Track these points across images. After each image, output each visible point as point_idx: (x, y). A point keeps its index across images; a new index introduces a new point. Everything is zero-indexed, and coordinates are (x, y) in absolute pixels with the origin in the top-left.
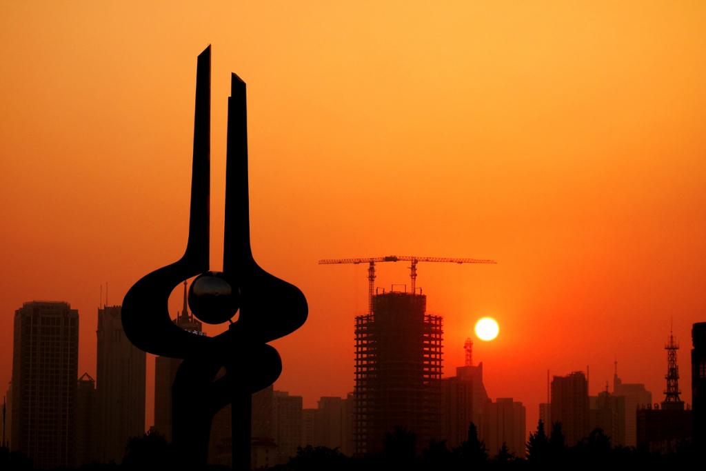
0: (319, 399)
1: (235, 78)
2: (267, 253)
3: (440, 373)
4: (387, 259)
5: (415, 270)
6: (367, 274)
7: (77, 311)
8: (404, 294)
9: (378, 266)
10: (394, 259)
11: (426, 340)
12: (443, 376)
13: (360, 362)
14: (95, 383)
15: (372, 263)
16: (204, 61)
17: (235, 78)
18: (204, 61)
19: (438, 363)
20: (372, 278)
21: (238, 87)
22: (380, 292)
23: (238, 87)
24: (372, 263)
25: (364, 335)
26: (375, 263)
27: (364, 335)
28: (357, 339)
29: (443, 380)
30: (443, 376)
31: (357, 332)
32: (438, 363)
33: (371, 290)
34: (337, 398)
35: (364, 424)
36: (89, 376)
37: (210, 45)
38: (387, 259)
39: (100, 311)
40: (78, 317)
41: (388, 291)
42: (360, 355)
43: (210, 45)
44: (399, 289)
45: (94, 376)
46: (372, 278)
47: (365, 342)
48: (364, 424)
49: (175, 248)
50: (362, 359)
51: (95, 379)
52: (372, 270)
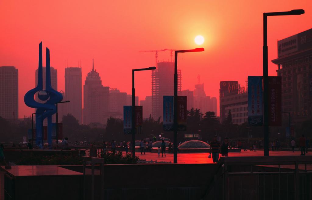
3: (181, 89)
5: (172, 54)
7: (56, 70)
8: (168, 62)
9: (158, 53)
10: (165, 50)
11: (189, 133)
12: (182, 90)
13: (153, 79)
14: (65, 94)
15: (157, 52)
16: (41, 45)
18: (41, 45)
19: (180, 81)
20: (157, 57)
21: (48, 51)
22: (160, 62)
23: (48, 51)
24: (157, 52)
25: (155, 76)
26: (158, 52)
27: (155, 76)
28: (152, 78)
30: (182, 90)
31: (152, 75)
32: (180, 88)
33: (156, 61)
35: (155, 93)
36: (62, 91)
39: (65, 69)
40: (57, 72)
41: (162, 61)
42: (153, 83)
44: (166, 61)
45: (64, 91)
46: (157, 57)
47: (155, 79)
48: (155, 99)
50: (154, 82)
51: (65, 92)
52: (156, 54)
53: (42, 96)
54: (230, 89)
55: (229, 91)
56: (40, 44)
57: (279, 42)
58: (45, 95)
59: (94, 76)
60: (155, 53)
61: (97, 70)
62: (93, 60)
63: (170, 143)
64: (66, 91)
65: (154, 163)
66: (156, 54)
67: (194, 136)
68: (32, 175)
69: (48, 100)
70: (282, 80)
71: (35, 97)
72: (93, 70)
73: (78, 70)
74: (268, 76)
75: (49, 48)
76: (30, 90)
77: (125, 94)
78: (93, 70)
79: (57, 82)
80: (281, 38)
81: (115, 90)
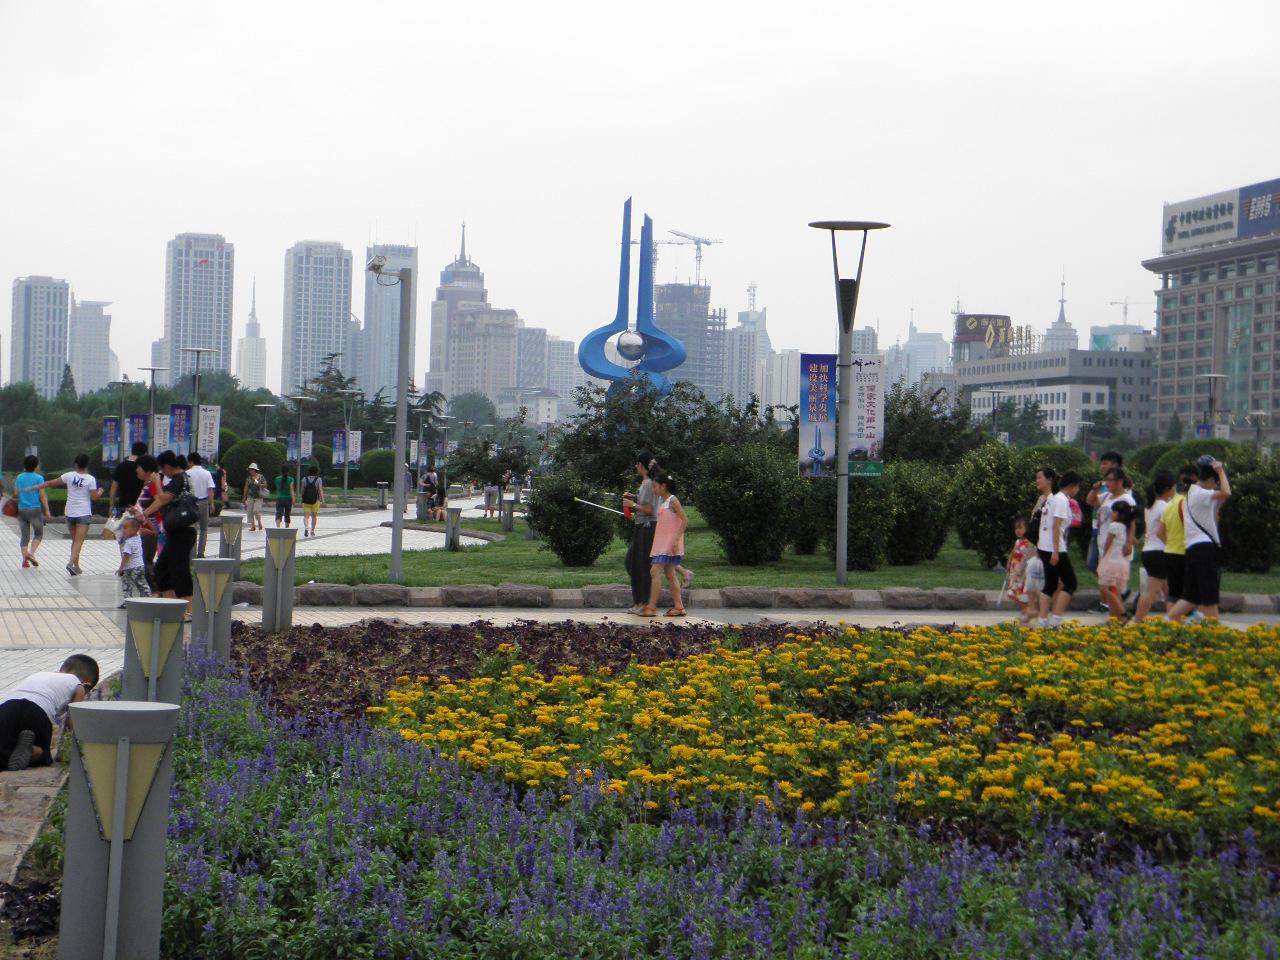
16: (628, 205)
18: (628, 205)
21: (648, 222)
23: (648, 222)
39: (369, 250)
52: (1126, 308)
53: (628, 347)
54: (992, 339)
55: (989, 345)
57: (1167, 208)
58: (638, 346)
59: (462, 277)
61: (475, 257)
62: (1062, 301)
66: (1126, 308)
68: (1121, 323)
70: (815, 773)
71: (612, 355)
72: (463, 255)
75: (651, 216)
77: (937, 337)
78: (463, 255)
79: (231, 314)
80: (1174, 200)
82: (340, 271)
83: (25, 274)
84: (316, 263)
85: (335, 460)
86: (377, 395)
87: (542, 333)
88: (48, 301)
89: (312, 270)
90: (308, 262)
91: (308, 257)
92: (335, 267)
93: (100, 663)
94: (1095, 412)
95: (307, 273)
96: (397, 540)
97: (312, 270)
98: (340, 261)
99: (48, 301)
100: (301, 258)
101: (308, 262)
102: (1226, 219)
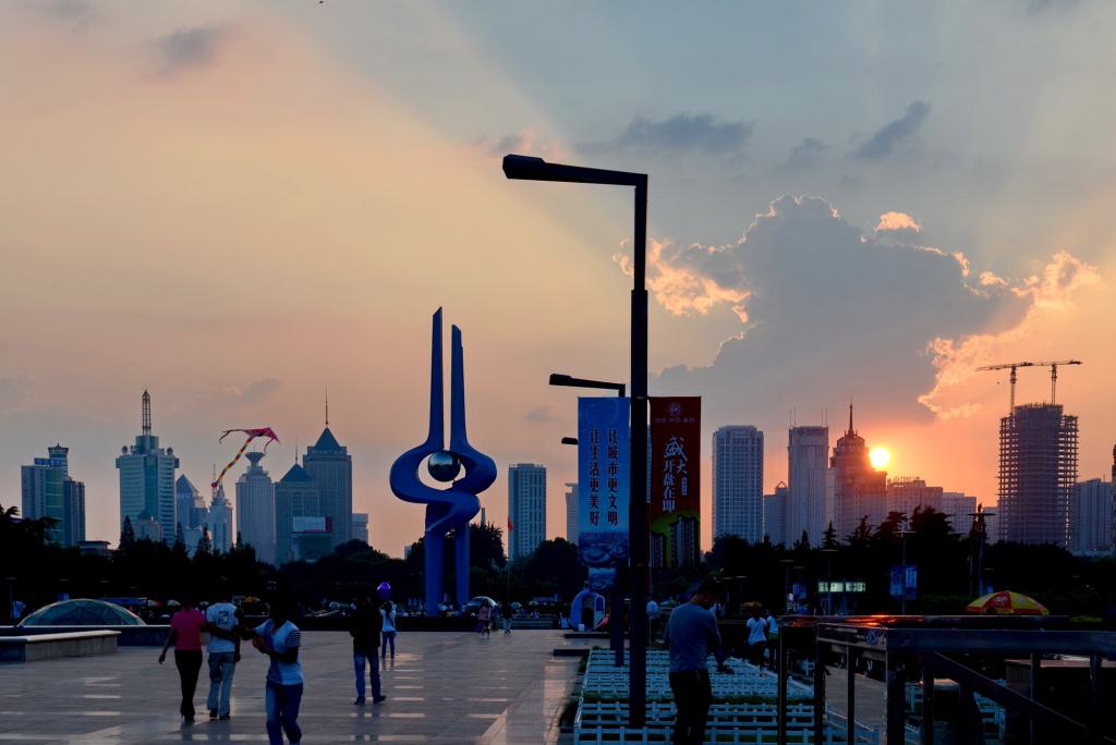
0: (495, 527)
1: (454, 327)
2: (476, 440)
4: (1025, 365)
6: (1009, 377)
11: (830, 580)
15: (1054, 366)
16: (437, 318)
17: (454, 327)
18: (437, 318)
21: (456, 333)
23: (456, 333)
29: (1079, 484)
30: (1079, 480)
31: (1001, 432)
34: (1092, 481)
37: (441, 308)
38: (1025, 365)
43: (441, 308)
49: (421, 436)
50: (1006, 455)
52: (1013, 373)
56: (434, 316)
60: (1010, 370)
63: (457, 607)
64: (790, 484)
65: (840, 645)
67: (845, 586)
69: (456, 479)
72: (851, 430)
73: (821, 432)
74: (634, 187)
76: (404, 455)
78: (851, 430)
81: (915, 481)
82: (753, 448)
83: (515, 463)
84: (734, 442)
85: (893, 592)
86: (863, 520)
87: (940, 490)
88: (531, 542)
89: (731, 449)
90: (728, 442)
91: (728, 438)
92: (750, 445)
93: (561, 536)
94: (756, 665)
95: (728, 450)
96: (237, 648)
97: (731, 449)
98: (753, 439)
99: (531, 542)
100: (722, 440)
101: (728, 442)
102: (594, 669)
